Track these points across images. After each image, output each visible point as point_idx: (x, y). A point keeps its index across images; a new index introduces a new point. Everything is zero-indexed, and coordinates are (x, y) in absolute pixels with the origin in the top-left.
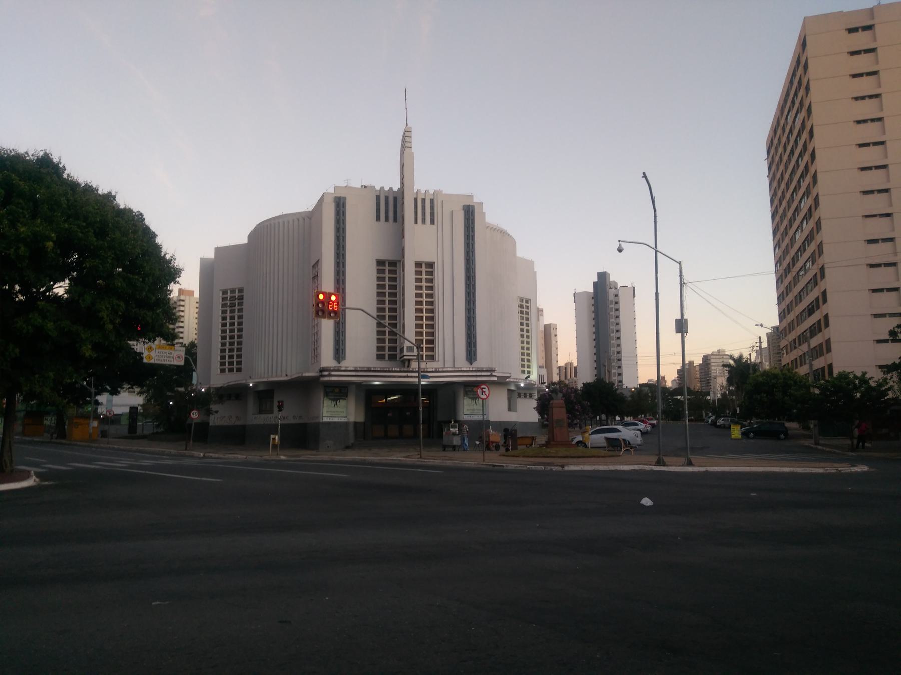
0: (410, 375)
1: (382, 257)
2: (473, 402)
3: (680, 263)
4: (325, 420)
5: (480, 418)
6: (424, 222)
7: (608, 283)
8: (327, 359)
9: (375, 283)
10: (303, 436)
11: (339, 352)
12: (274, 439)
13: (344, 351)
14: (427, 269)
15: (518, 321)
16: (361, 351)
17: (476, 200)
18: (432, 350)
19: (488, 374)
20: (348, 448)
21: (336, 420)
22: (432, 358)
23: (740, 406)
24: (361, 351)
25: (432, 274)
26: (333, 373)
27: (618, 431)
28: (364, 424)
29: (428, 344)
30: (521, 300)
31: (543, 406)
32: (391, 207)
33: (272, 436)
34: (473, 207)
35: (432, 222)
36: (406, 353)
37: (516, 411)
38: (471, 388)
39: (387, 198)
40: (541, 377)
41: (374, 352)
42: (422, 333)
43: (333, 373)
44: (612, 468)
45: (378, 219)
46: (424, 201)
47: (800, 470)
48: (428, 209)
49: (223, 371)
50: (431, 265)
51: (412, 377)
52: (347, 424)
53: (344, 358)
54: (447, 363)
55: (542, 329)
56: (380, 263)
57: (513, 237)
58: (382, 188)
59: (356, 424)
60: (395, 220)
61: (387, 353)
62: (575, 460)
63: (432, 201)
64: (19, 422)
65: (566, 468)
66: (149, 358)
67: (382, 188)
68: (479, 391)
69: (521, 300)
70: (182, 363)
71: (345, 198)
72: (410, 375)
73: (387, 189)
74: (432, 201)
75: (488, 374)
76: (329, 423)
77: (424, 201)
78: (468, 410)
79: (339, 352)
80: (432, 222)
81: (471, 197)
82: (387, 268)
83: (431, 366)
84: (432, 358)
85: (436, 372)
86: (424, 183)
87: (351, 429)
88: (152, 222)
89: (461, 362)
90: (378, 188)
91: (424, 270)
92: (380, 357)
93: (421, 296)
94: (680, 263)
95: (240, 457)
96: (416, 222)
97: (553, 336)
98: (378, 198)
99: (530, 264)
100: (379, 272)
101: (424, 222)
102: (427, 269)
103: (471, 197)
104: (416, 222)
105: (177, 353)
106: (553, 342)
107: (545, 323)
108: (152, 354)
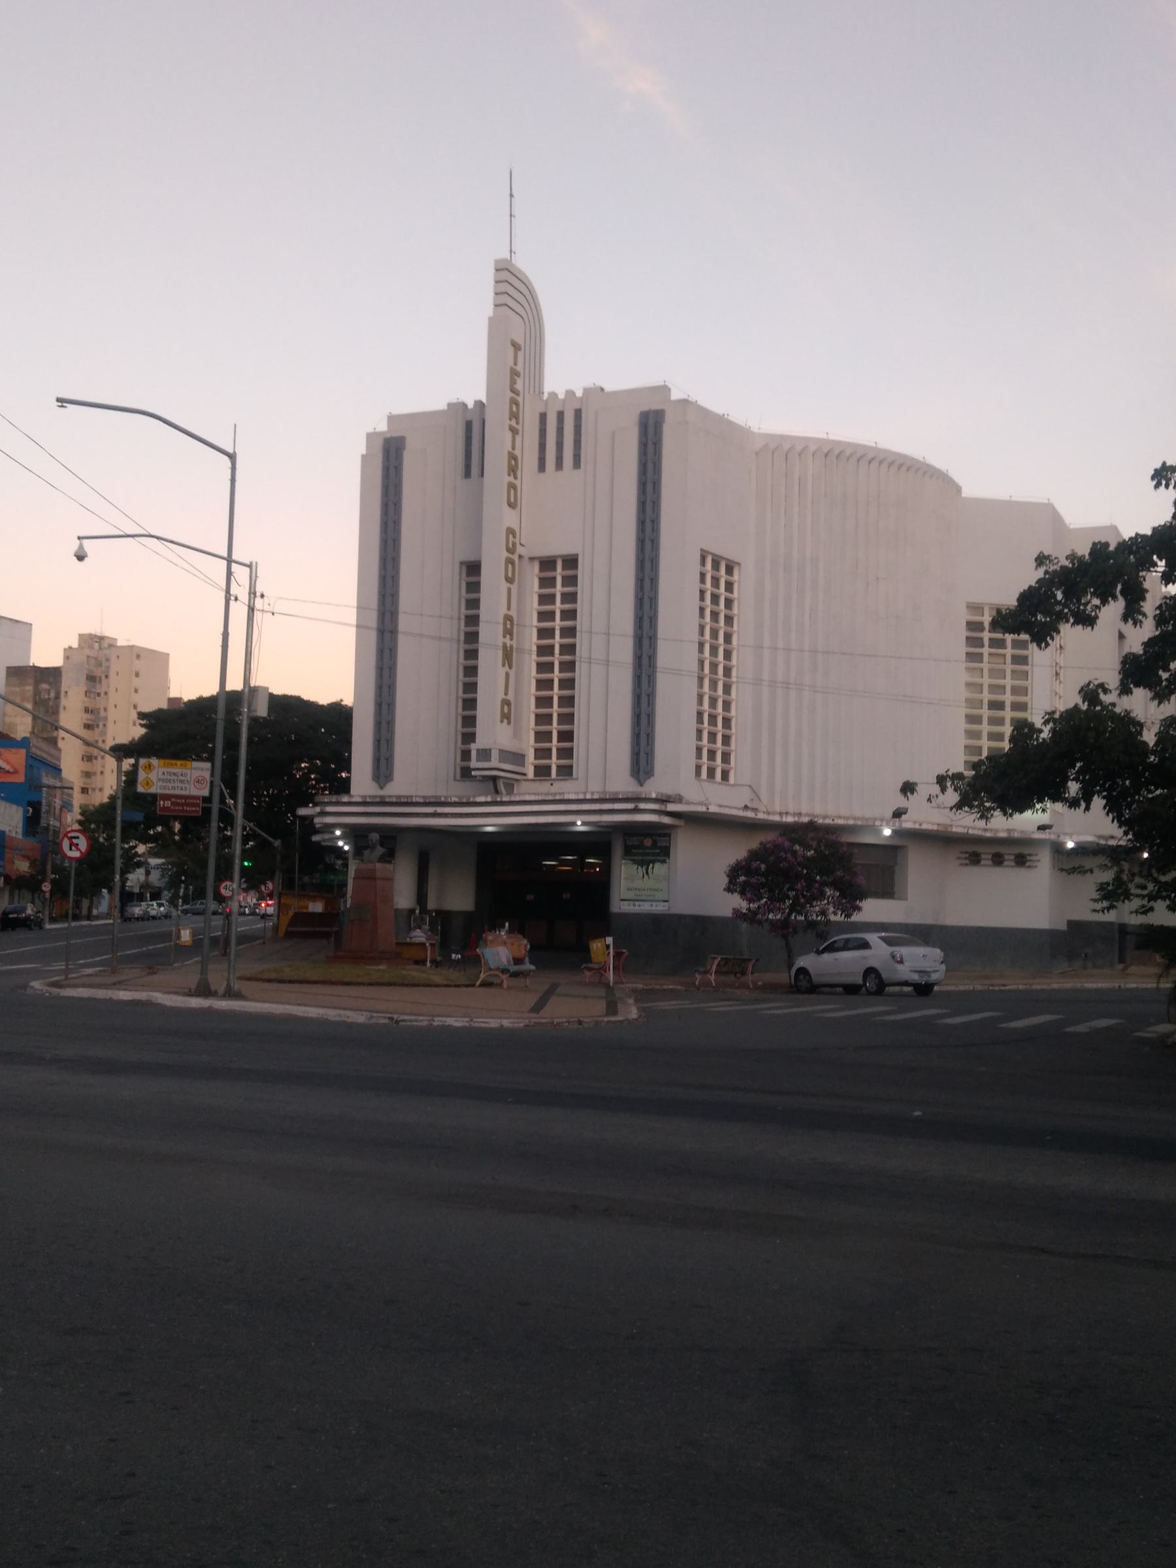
0: (440, 810)
2: (642, 870)
3: (232, 457)
6: (559, 465)
13: (389, 760)
14: (559, 571)
19: (630, 806)
22: (566, 772)
23: (504, 926)
26: (642, 806)
27: (865, 945)
28: (471, 913)
31: (741, 877)
35: (577, 464)
36: (474, 763)
37: (904, 898)
38: (649, 843)
39: (561, 415)
43: (642, 806)
46: (561, 415)
48: (564, 433)
50: (571, 562)
51: (446, 815)
53: (650, 773)
54: (594, 784)
57: (937, 460)
61: (554, 761)
63: (578, 414)
66: (148, 783)
67: (570, 393)
72: (440, 810)
74: (578, 414)
75: (630, 806)
78: (632, 890)
80: (577, 464)
81: (664, 390)
83: (568, 789)
86: (563, 375)
89: (622, 783)
94: (232, 457)
95: (451, 1021)
96: (542, 467)
99: (1154, 529)
101: (559, 465)
102: (559, 571)
104: (542, 467)
105: (196, 774)
108: (153, 776)
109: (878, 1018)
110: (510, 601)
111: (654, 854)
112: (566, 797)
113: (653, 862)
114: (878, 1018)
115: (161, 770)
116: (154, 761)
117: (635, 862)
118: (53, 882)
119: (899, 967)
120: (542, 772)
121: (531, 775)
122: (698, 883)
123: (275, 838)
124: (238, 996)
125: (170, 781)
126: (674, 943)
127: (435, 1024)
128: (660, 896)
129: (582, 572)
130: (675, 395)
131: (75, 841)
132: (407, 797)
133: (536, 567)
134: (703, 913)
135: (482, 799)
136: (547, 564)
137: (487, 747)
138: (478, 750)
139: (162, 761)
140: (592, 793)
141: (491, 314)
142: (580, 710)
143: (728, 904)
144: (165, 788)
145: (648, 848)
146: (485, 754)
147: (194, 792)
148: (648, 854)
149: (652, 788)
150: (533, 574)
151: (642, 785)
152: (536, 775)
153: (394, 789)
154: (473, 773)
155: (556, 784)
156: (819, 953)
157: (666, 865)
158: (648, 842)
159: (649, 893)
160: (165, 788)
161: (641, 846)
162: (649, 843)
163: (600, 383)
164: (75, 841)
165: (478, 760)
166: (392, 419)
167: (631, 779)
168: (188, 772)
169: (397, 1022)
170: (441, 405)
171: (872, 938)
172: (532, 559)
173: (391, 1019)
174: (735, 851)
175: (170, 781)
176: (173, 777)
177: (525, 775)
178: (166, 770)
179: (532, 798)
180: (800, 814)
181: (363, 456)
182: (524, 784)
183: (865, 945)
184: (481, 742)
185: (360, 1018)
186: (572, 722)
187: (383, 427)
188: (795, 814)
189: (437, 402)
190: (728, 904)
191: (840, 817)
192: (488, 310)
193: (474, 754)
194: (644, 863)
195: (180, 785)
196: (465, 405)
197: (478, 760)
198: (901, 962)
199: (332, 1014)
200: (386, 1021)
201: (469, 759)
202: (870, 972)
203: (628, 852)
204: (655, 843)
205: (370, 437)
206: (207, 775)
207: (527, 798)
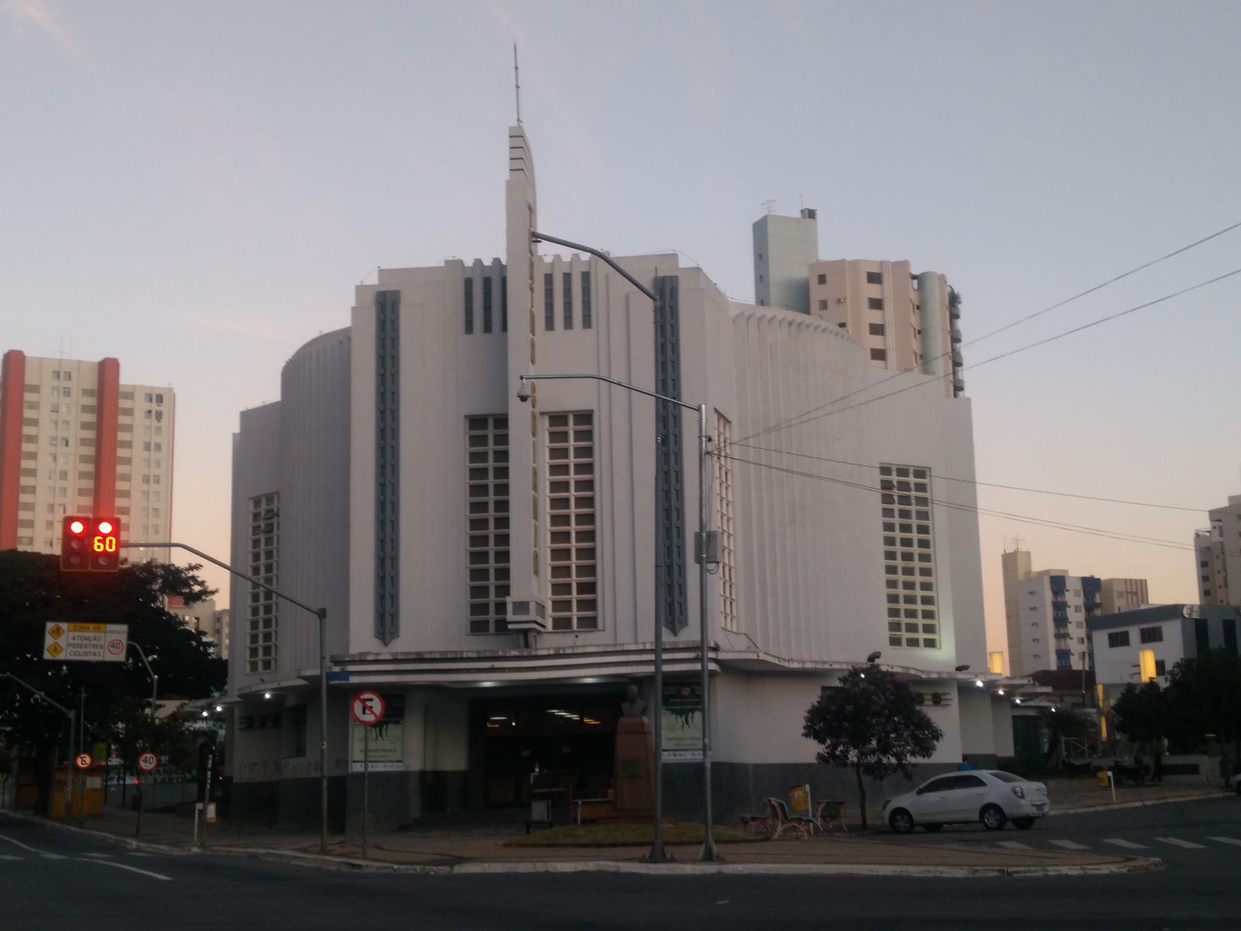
0: (497, 664)
2: (680, 720)
4: (358, 768)
5: (697, 757)
6: (568, 324)
9: (464, 464)
10: (331, 805)
12: (203, 813)
13: (395, 617)
14: (573, 429)
17: (684, 263)
18: (592, 605)
20: (403, 828)
21: (379, 768)
22: (590, 623)
24: (433, 614)
25: (588, 435)
26: (351, 668)
27: (977, 782)
29: (580, 594)
30: (885, 470)
31: (822, 722)
32: (483, 298)
33: (199, 806)
34: (674, 279)
35: (587, 323)
36: (510, 616)
38: (684, 693)
39: (567, 277)
41: (463, 615)
43: (351, 668)
44: (540, 867)
45: (469, 328)
46: (567, 277)
48: (572, 295)
49: (254, 666)
50: (585, 417)
51: (502, 670)
52: (403, 776)
53: (395, 633)
54: (620, 637)
58: (478, 262)
60: (488, 328)
64: (1119, 760)
65: (458, 869)
66: (56, 649)
67: (478, 262)
68: (358, 706)
69: (885, 470)
70: (120, 657)
72: (497, 664)
73: (488, 262)
80: (587, 323)
82: (571, 428)
83: (590, 640)
84: (590, 623)
85: (557, 656)
88: (288, 353)
90: (469, 263)
91: (571, 428)
92: (478, 628)
93: (564, 486)
95: (1065, 870)
96: (550, 325)
98: (468, 283)
100: (474, 441)
101: (568, 324)
102: (573, 429)
104: (550, 325)
105: (110, 637)
108: (62, 641)
109: (1082, 847)
111: (693, 703)
112: (382, 657)
113: (693, 711)
114: (1082, 847)
115: (71, 634)
117: (673, 712)
119: (1022, 802)
120: (562, 624)
121: (550, 627)
122: (771, 734)
123: (69, 707)
124: (721, 860)
125: (80, 646)
127: (1051, 873)
128: (393, 756)
129: (599, 427)
131: (369, 703)
132: (456, 652)
133: (546, 420)
134: (734, 761)
135: (514, 653)
136: (558, 419)
137: (524, 600)
138: (514, 603)
139: (72, 625)
140: (644, 644)
141: (508, 177)
142: (603, 561)
143: (809, 751)
144: (75, 654)
145: (686, 697)
146: (522, 607)
148: (686, 704)
151: (675, 634)
152: (554, 628)
154: (510, 627)
155: (581, 636)
156: (921, 792)
157: (400, 727)
158: (686, 691)
159: (689, 742)
160: (75, 654)
163: (459, 256)
164: (369, 703)
165: (514, 614)
166: (382, 272)
167: (376, 640)
168: (102, 635)
169: (1009, 874)
170: (437, 261)
172: (542, 414)
173: (1002, 871)
174: (810, 697)
175: (80, 646)
176: (87, 642)
177: (543, 626)
178: (76, 634)
179: (594, 649)
180: (804, 662)
181: (353, 309)
182: (546, 636)
183: (977, 782)
185: (960, 873)
186: (508, 578)
187: (373, 280)
188: (798, 662)
189: (435, 259)
190: (809, 751)
191: (835, 663)
193: (510, 608)
195: (93, 650)
196: (461, 262)
197: (514, 614)
198: (1022, 797)
199: (914, 871)
200: (997, 874)
201: (505, 612)
202: (989, 808)
203: (667, 701)
204: (693, 691)
205: (360, 289)
206: (123, 638)
207: (590, 650)
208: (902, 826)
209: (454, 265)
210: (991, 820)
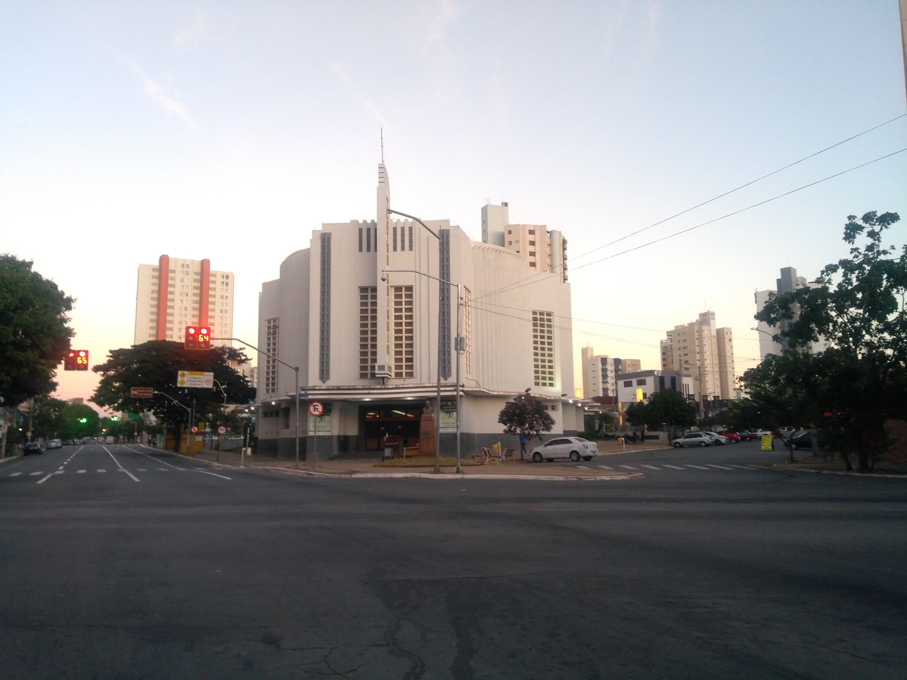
1: (364, 285)
2: (447, 415)
4: (311, 434)
6: (403, 248)
7: (793, 279)
8: (314, 379)
11: (324, 374)
12: (245, 452)
15: (532, 333)
16: (344, 371)
17: (452, 224)
20: (331, 459)
21: (321, 434)
22: (410, 375)
24: (344, 371)
25: (411, 296)
27: (569, 442)
28: (357, 436)
30: (534, 313)
31: (507, 417)
32: (367, 237)
34: (448, 231)
35: (411, 248)
36: (377, 371)
38: (449, 404)
40: (586, 392)
42: (401, 352)
44: (388, 475)
45: (361, 250)
46: (403, 229)
47: (542, 478)
48: (404, 237)
49: (268, 391)
50: (410, 288)
52: (331, 437)
53: (328, 378)
54: (423, 381)
55: (714, 333)
56: (363, 289)
58: (365, 221)
59: (339, 437)
60: (369, 250)
62: (402, 469)
65: (353, 476)
66: (183, 382)
67: (365, 221)
68: (312, 408)
69: (534, 313)
71: (330, 234)
73: (369, 221)
76: (312, 437)
77: (403, 229)
79: (324, 374)
80: (411, 248)
83: (410, 382)
84: (410, 375)
85: (396, 388)
87: (335, 441)
90: (361, 222)
91: (404, 293)
92: (363, 376)
95: (604, 478)
96: (395, 249)
97: (727, 340)
98: (361, 230)
100: (363, 297)
101: (403, 248)
102: (404, 294)
103: (448, 221)
104: (395, 249)
105: (206, 378)
106: (728, 347)
107: (718, 326)
108: (185, 379)
110: (385, 303)
116: (186, 372)
118: (32, 432)
122: (485, 421)
124: (463, 473)
126: (468, 447)
130: (452, 224)
136: (398, 289)
143: (501, 428)
146: (382, 368)
147: (205, 386)
149: (452, 380)
150: (392, 291)
153: (332, 382)
158: (450, 403)
161: (447, 405)
162: (449, 404)
171: (571, 438)
174: (501, 406)
183: (569, 442)
184: (380, 362)
185: (561, 479)
187: (320, 228)
189: (346, 220)
192: (377, 184)
193: (377, 368)
194: (449, 412)
206: (212, 378)
208: (538, 459)
209: (355, 222)
210: (574, 457)
